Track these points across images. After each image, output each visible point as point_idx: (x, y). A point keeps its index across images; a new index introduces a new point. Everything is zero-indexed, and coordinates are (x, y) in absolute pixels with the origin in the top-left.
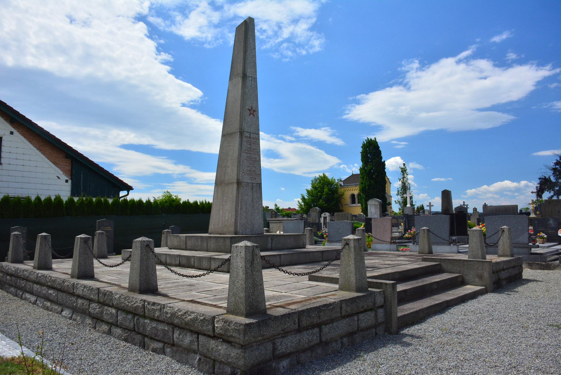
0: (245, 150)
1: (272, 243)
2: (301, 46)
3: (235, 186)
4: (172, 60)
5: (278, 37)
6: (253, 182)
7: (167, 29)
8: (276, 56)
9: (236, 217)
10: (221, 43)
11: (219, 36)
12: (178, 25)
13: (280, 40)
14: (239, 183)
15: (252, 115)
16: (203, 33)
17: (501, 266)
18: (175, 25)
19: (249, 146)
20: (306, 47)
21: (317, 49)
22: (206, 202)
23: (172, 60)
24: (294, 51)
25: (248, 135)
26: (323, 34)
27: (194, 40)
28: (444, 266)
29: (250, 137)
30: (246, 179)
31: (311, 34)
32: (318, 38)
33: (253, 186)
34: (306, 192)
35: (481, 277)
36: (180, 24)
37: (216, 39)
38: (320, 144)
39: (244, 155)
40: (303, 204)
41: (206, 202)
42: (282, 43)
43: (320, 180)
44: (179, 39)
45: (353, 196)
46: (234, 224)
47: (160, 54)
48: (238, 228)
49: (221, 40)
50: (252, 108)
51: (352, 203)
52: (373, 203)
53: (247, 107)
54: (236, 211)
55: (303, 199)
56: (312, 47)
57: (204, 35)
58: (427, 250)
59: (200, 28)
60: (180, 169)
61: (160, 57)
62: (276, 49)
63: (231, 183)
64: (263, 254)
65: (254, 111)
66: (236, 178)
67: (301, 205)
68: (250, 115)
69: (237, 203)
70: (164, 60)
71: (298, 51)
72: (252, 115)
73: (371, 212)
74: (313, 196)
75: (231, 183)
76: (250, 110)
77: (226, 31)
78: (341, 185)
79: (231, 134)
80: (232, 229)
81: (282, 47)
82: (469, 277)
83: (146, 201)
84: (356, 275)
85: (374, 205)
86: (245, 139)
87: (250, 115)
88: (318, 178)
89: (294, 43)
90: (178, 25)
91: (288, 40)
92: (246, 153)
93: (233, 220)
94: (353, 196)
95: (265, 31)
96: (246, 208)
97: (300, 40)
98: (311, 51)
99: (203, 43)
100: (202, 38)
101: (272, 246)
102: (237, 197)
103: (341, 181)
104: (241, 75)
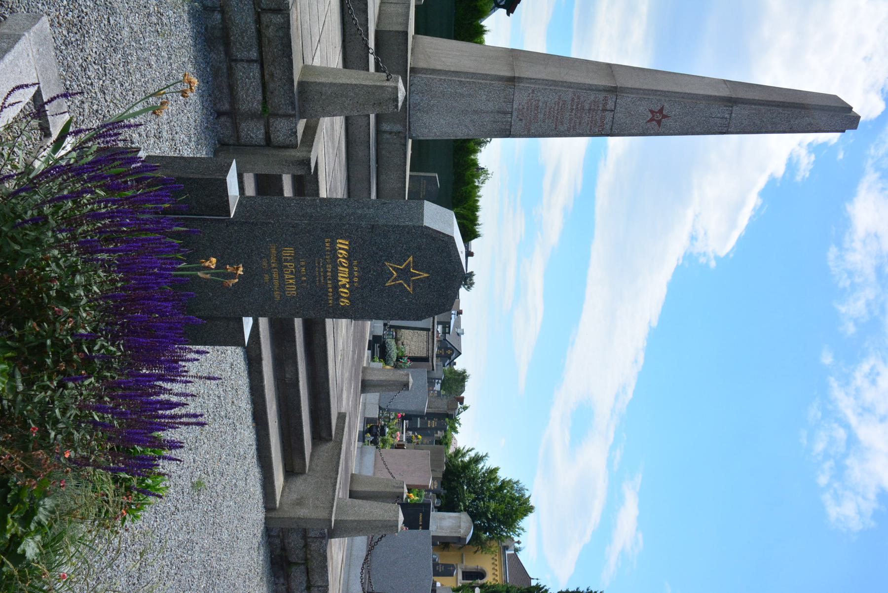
0: (579, 98)
1: (390, 133)
2: (840, 471)
3: (508, 74)
4: (798, 178)
5: (860, 414)
6: (515, 114)
7: (870, 162)
8: (814, 412)
9: (446, 73)
10: (841, 285)
11: (858, 280)
12: (880, 185)
13: (853, 420)
14: (512, 80)
15: (650, 116)
16: (864, 242)
17: (316, 579)
18: (880, 178)
19: (587, 107)
20: (836, 485)
21: (833, 511)
22: (480, 197)
23: (798, 178)
24: (826, 456)
25: (611, 105)
26: (873, 524)
27: (845, 223)
28: (326, 448)
29: (604, 110)
30: (521, 98)
31: (872, 496)
32: (860, 513)
33: (505, 113)
34: (493, 467)
35: (300, 503)
36: (883, 189)
37: (850, 274)
38: (606, 529)
39: (568, 95)
40: (467, 459)
41: (480, 197)
42: (847, 426)
43: (518, 499)
44: (848, 190)
45: (481, 575)
46: (432, 67)
47: (810, 152)
48: (424, 76)
49: (848, 283)
50: (665, 117)
51: (463, 572)
52: (463, 525)
53: (666, 105)
54: (457, 73)
55: (477, 460)
56: (838, 499)
57: (857, 245)
58: (358, 488)
59: (876, 235)
60: (554, 220)
61: (803, 152)
62: (831, 414)
63: (513, 70)
64: (372, 117)
65: (659, 123)
66: (522, 76)
67: (464, 455)
68: (652, 112)
69: (473, 75)
70: (798, 161)
71: (828, 465)
72: (650, 116)
73: (442, 519)
74: (483, 482)
75: (513, 70)
76: (661, 111)
77: (870, 293)
78: (506, 548)
79: (614, 76)
80: (422, 64)
81: (835, 425)
82: (300, 484)
83: (482, 27)
84: (332, 85)
85: (460, 527)
86: (601, 96)
87: (652, 112)
88: (523, 495)
89: (846, 455)
90: (880, 185)
91: (852, 441)
92: (573, 100)
93: (439, 67)
94: (481, 575)
95: (874, 382)
96: (462, 95)
97: (855, 469)
98: (827, 497)
99: (839, 244)
100: (852, 241)
101: (385, 132)
102: (485, 76)
103: (516, 550)
104: (734, 96)
